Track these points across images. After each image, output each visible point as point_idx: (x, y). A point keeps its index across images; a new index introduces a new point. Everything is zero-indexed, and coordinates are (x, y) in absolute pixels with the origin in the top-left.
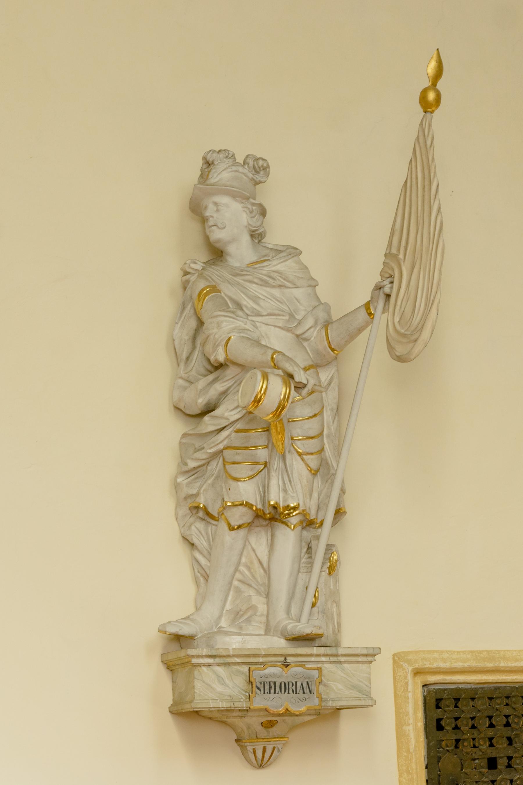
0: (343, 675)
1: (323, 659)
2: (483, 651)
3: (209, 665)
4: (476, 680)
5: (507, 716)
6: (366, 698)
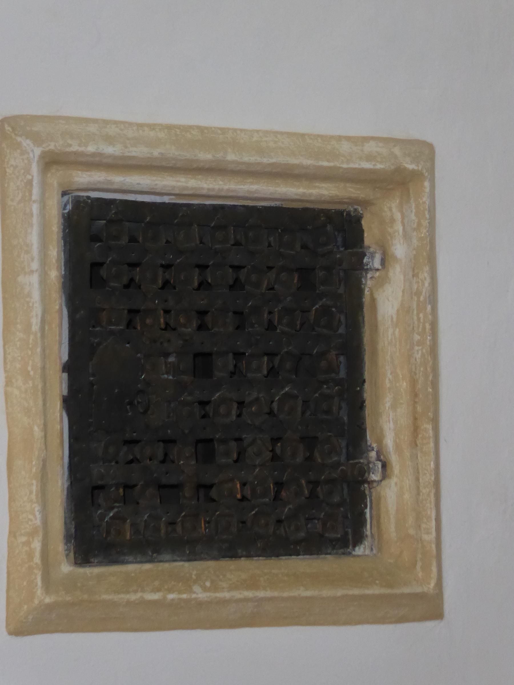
4: (174, 187)
5: (237, 268)
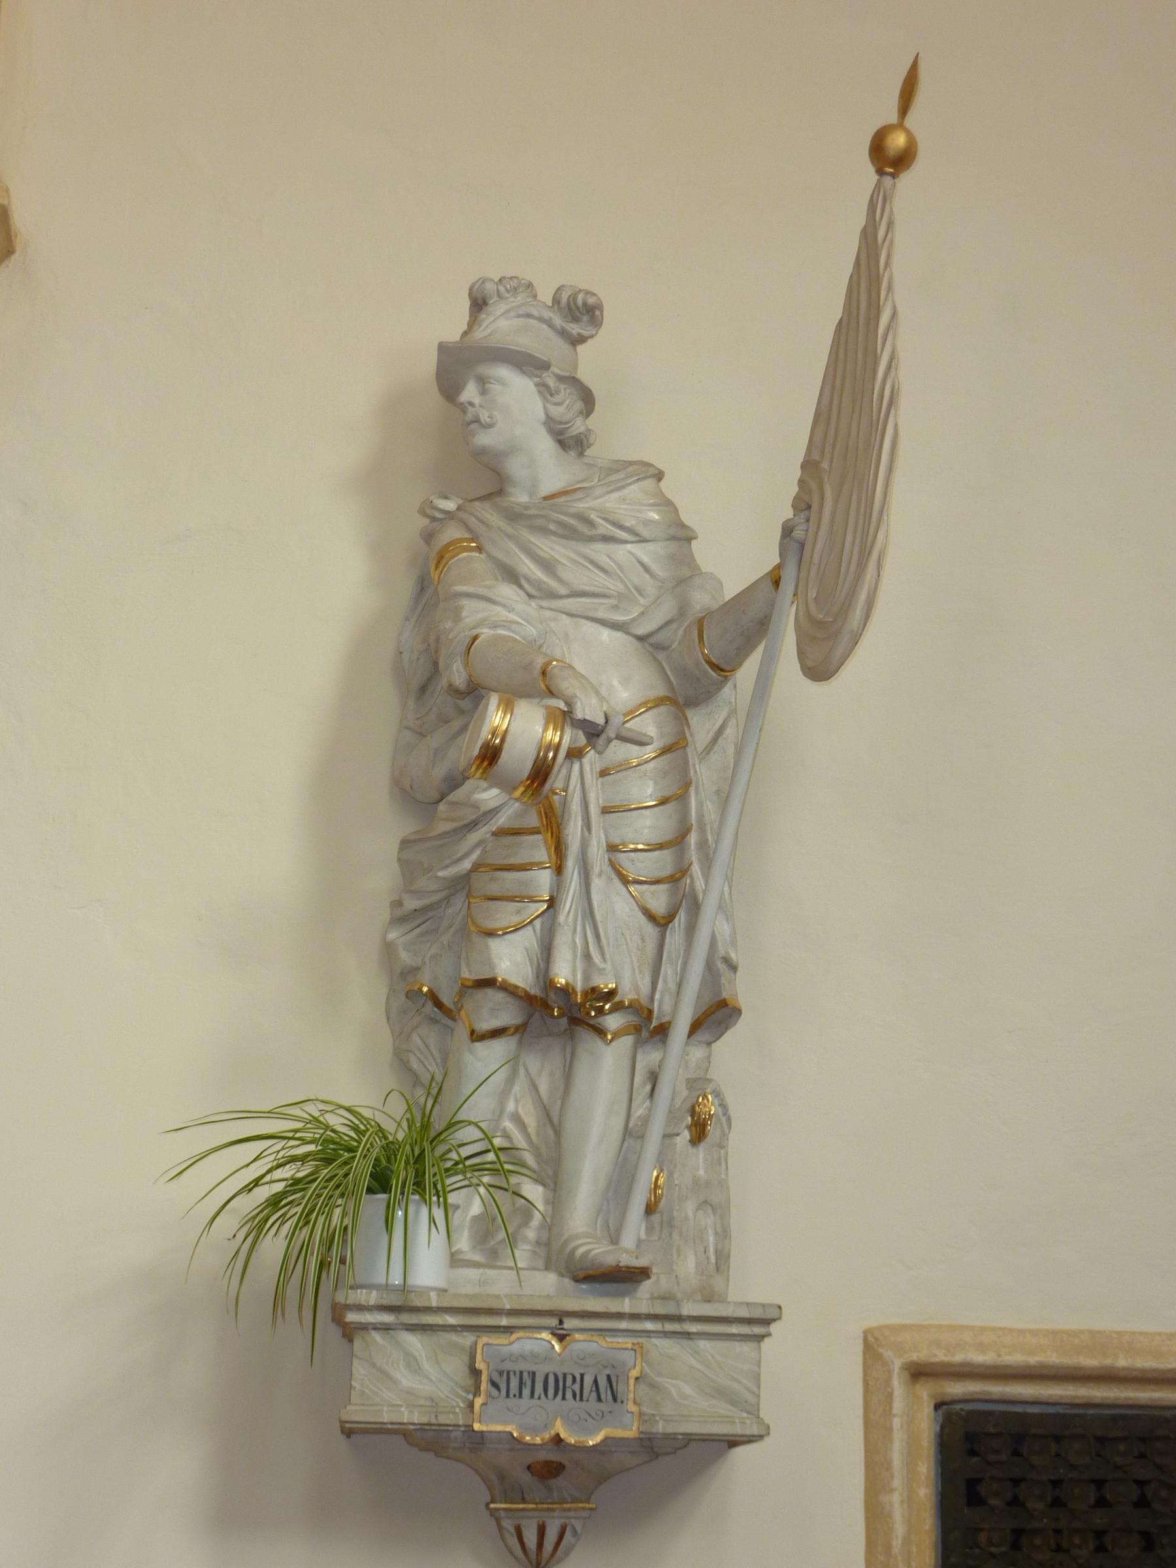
0: (694, 1363)
1: (649, 1326)
2: (1081, 1332)
3: (386, 1328)
4: (1062, 1397)
5: (1141, 1483)
6: (748, 1418)
